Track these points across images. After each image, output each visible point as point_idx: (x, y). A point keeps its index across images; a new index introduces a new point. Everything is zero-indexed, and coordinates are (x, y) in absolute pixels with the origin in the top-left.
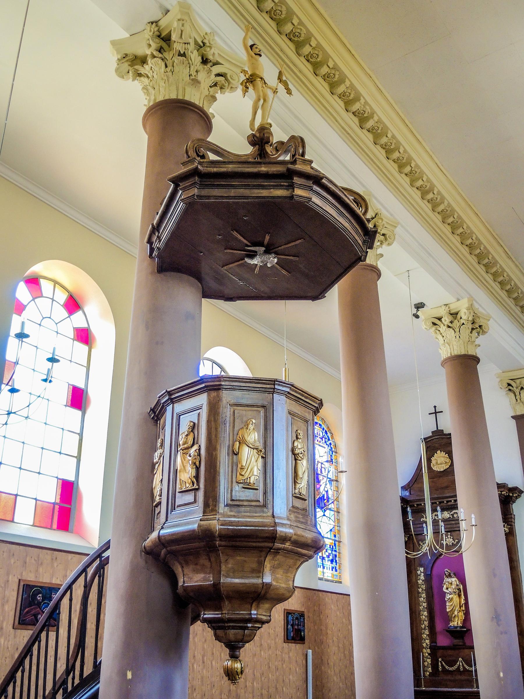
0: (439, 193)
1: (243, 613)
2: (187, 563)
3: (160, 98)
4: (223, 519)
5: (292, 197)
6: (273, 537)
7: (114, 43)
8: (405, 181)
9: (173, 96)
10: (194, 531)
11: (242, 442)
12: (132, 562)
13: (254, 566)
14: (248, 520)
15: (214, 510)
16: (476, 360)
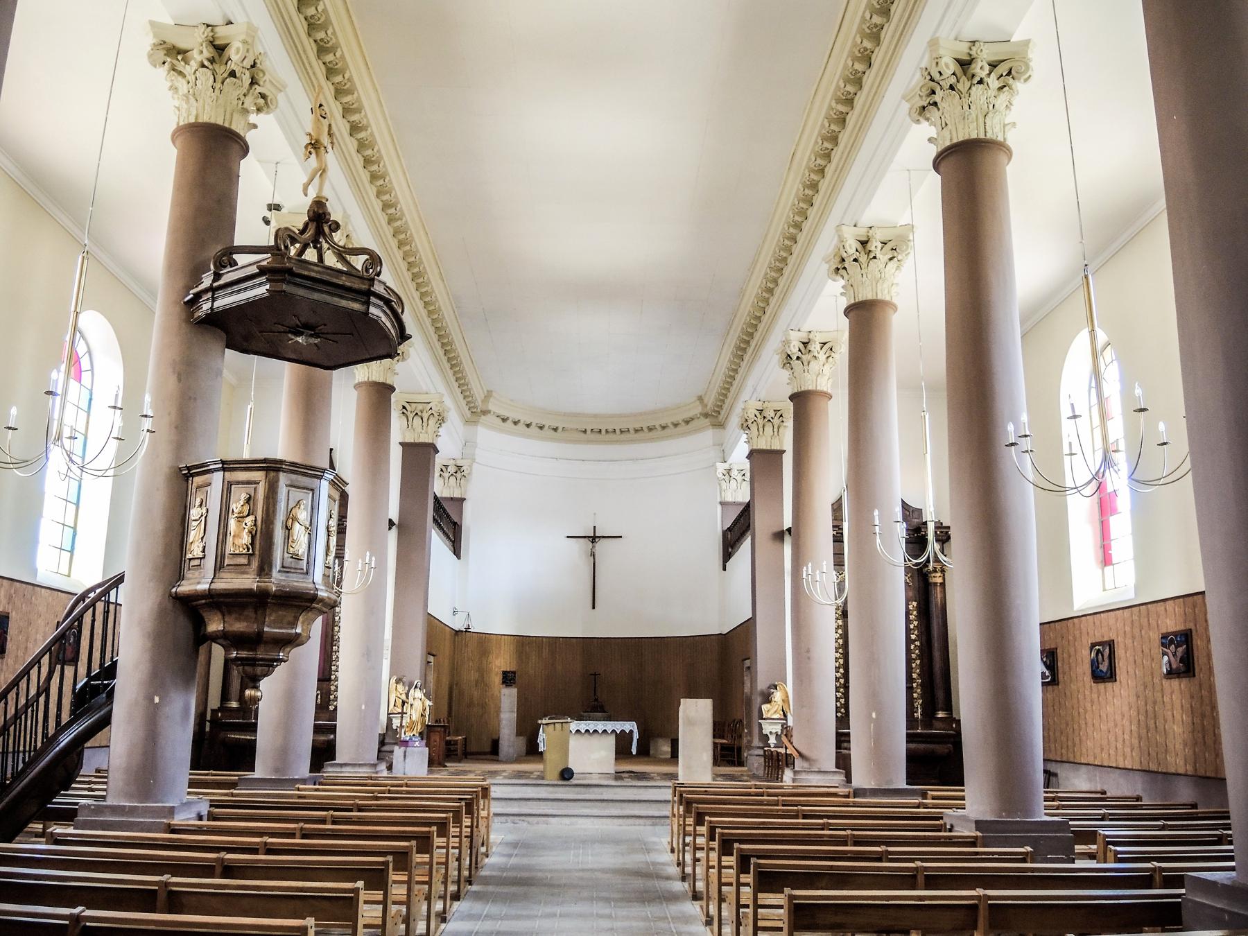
0: (401, 210)
1: (273, 655)
2: (230, 613)
3: (204, 118)
4: (276, 580)
5: (367, 313)
6: (313, 598)
7: (153, 24)
8: (372, 191)
9: (220, 122)
11: (295, 519)
12: (160, 604)
13: (291, 619)
14: (297, 582)
15: (269, 575)
16: (392, 389)
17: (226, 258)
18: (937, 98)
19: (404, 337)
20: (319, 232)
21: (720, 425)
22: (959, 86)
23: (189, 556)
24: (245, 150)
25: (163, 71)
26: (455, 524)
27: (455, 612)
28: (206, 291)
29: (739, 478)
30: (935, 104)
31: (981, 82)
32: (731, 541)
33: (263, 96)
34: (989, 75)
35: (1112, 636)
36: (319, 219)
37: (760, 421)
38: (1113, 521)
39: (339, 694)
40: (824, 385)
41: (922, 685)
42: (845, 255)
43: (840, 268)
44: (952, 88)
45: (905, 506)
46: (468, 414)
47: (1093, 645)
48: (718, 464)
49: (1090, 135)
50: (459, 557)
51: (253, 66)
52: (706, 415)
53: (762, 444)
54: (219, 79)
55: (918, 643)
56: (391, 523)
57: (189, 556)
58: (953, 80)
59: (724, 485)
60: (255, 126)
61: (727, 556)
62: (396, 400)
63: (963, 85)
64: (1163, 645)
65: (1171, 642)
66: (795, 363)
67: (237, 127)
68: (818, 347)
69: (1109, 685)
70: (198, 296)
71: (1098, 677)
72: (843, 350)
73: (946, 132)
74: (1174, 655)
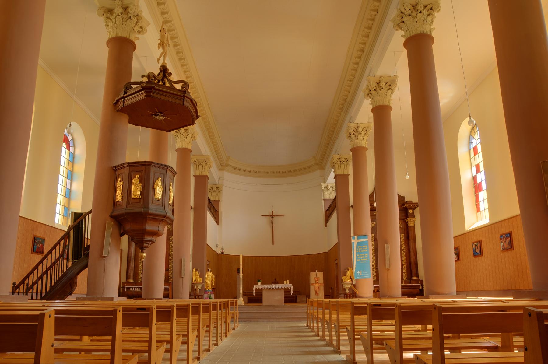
3: (120, 35)
9: (125, 36)
17: (128, 87)
18: (404, 20)
19: (198, 117)
20: (164, 76)
21: (323, 168)
22: (413, 14)
23: (117, 201)
24: (134, 47)
25: (103, 19)
26: (216, 210)
27: (217, 246)
28: (121, 98)
29: (331, 189)
30: (403, 22)
31: (420, 12)
32: (328, 215)
33: (141, 28)
34: (424, 10)
35: (481, 238)
36: (164, 70)
37: (339, 163)
38: (480, 194)
39: (173, 260)
40: (364, 144)
41: (407, 267)
42: (370, 88)
43: (369, 94)
44: (409, 15)
45: (399, 196)
46: (220, 166)
47: (474, 243)
48: (322, 184)
49: (466, 41)
50: (218, 224)
51: (138, 15)
52: (317, 164)
53: (340, 172)
54: (125, 20)
55: (405, 250)
56: (191, 208)
57: (117, 201)
58: (410, 12)
59: (325, 192)
60: (138, 39)
61: (327, 221)
62: (193, 158)
63: (414, 14)
64: (501, 239)
65: (504, 237)
66: (353, 136)
67: (132, 38)
68: (361, 129)
69: (480, 258)
70: (118, 101)
71: (475, 255)
72: (371, 131)
73: (408, 32)
74: (505, 242)
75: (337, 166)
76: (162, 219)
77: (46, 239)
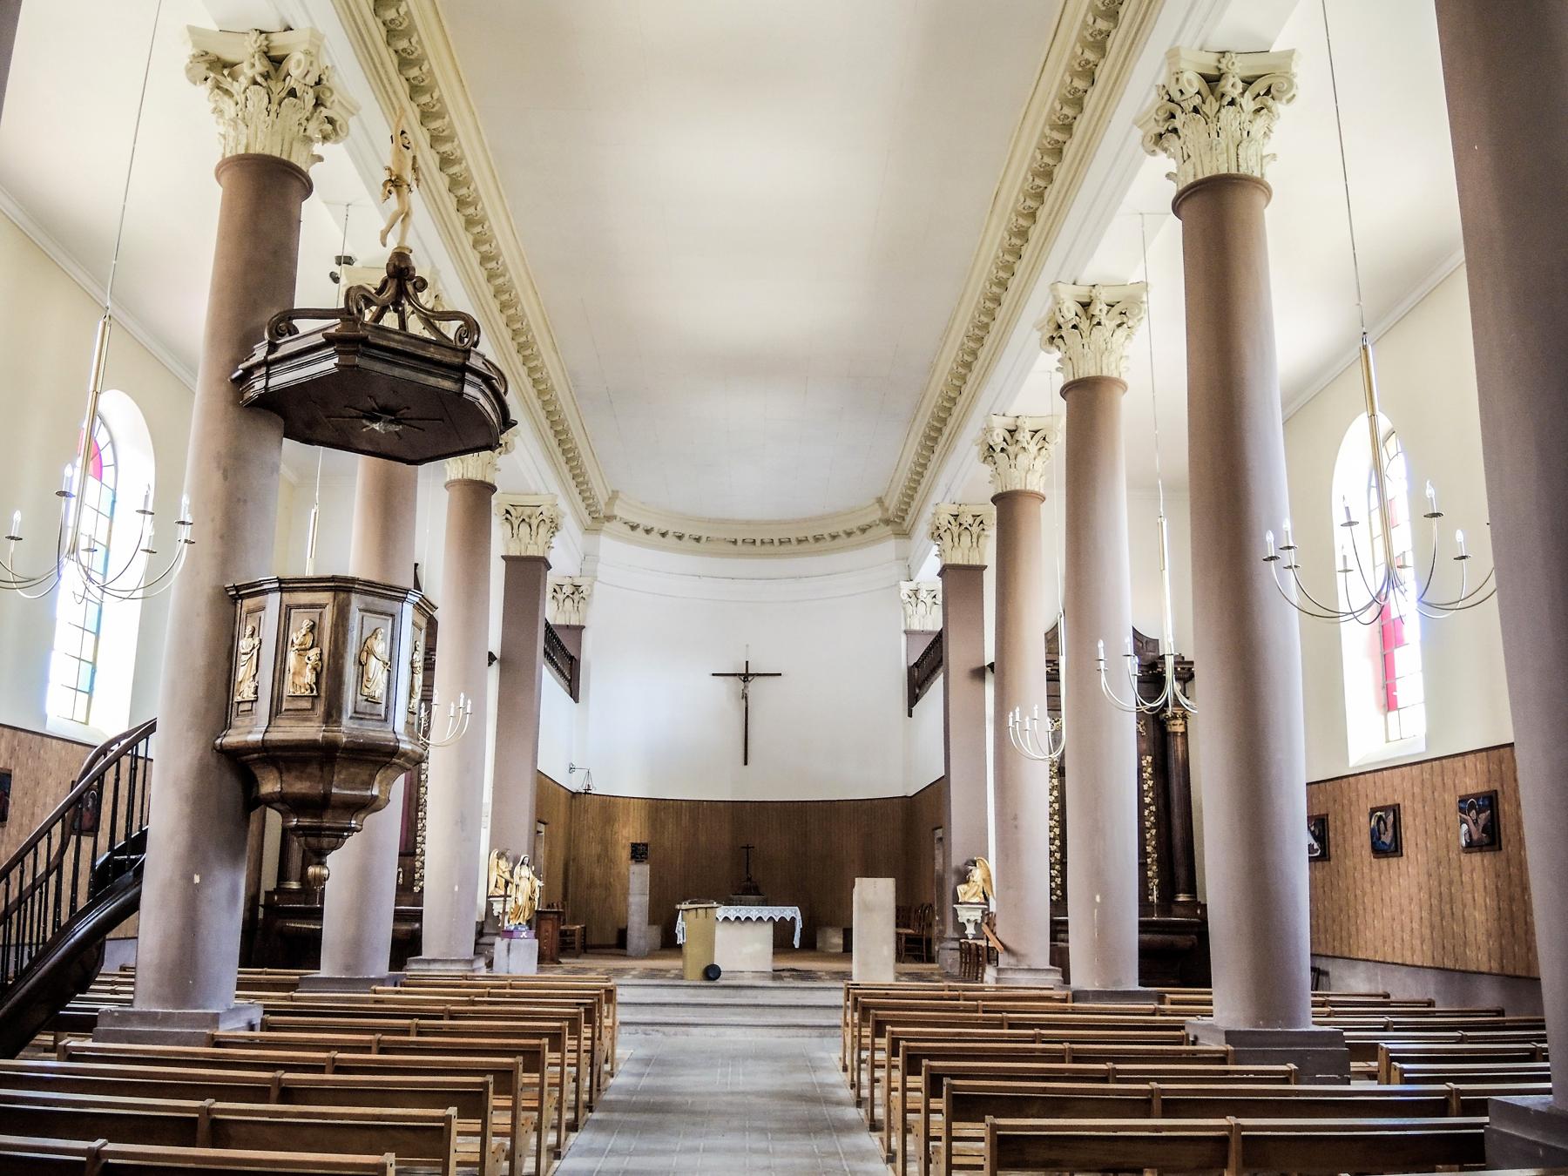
0: (504, 263)
1: (343, 823)
2: (289, 770)
3: (257, 149)
4: (347, 729)
5: (461, 393)
6: (394, 752)
7: (192, 30)
8: (467, 240)
9: (276, 153)
10: (316, 741)
11: (370, 652)
12: (201, 758)
13: (365, 777)
14: (373, 732)
15: (338, 722)
16: (493, 489)
18: (1177, 123)
19: (507, 423)
20: (401, 292)
21: (905, 534)
22: (1205, 108)
24: (307, 188)
25: (204, 89)
26: (572, 658)
27: (572, 769)
29: (929, 601)
30: (1175, 131)
31: (1232, 103)
32: (918, 680)
33: (331, 121)
34: (1243, 94)
35: (1398, 799)
37: (955, 529)
38: (1399, 654)
40: (1035, 483)
41: (1159, 861)
42: (1061, 321)
43: (1055, 337)
44: (1196, 110)
45: (1137, 635)
46: (588, 520)
47: (1373, 811)
48: (902, 583)
50: (576, 700)
52: (887, 522)
53: (958, 558)
54: (275, 99)
55: (1153, 808)
56: (491, 657)
58: (1197, 100)
59: (909, 609)
60: (320, 159)
61: (913, 699)
62: (497, 502)
63: (1210, 107)
64: (1461, 810)
65: (1472, 806)
66: (999, 456)
67: (298, 160)
68: (1028, 436)
69: (1394, 860)
71: (1379, 850)
72: (1059, 440)
73: (1189, 166)
74: (1476, 822)
75: (947, 537)
76: (378, 757)
77: (16, 773)
